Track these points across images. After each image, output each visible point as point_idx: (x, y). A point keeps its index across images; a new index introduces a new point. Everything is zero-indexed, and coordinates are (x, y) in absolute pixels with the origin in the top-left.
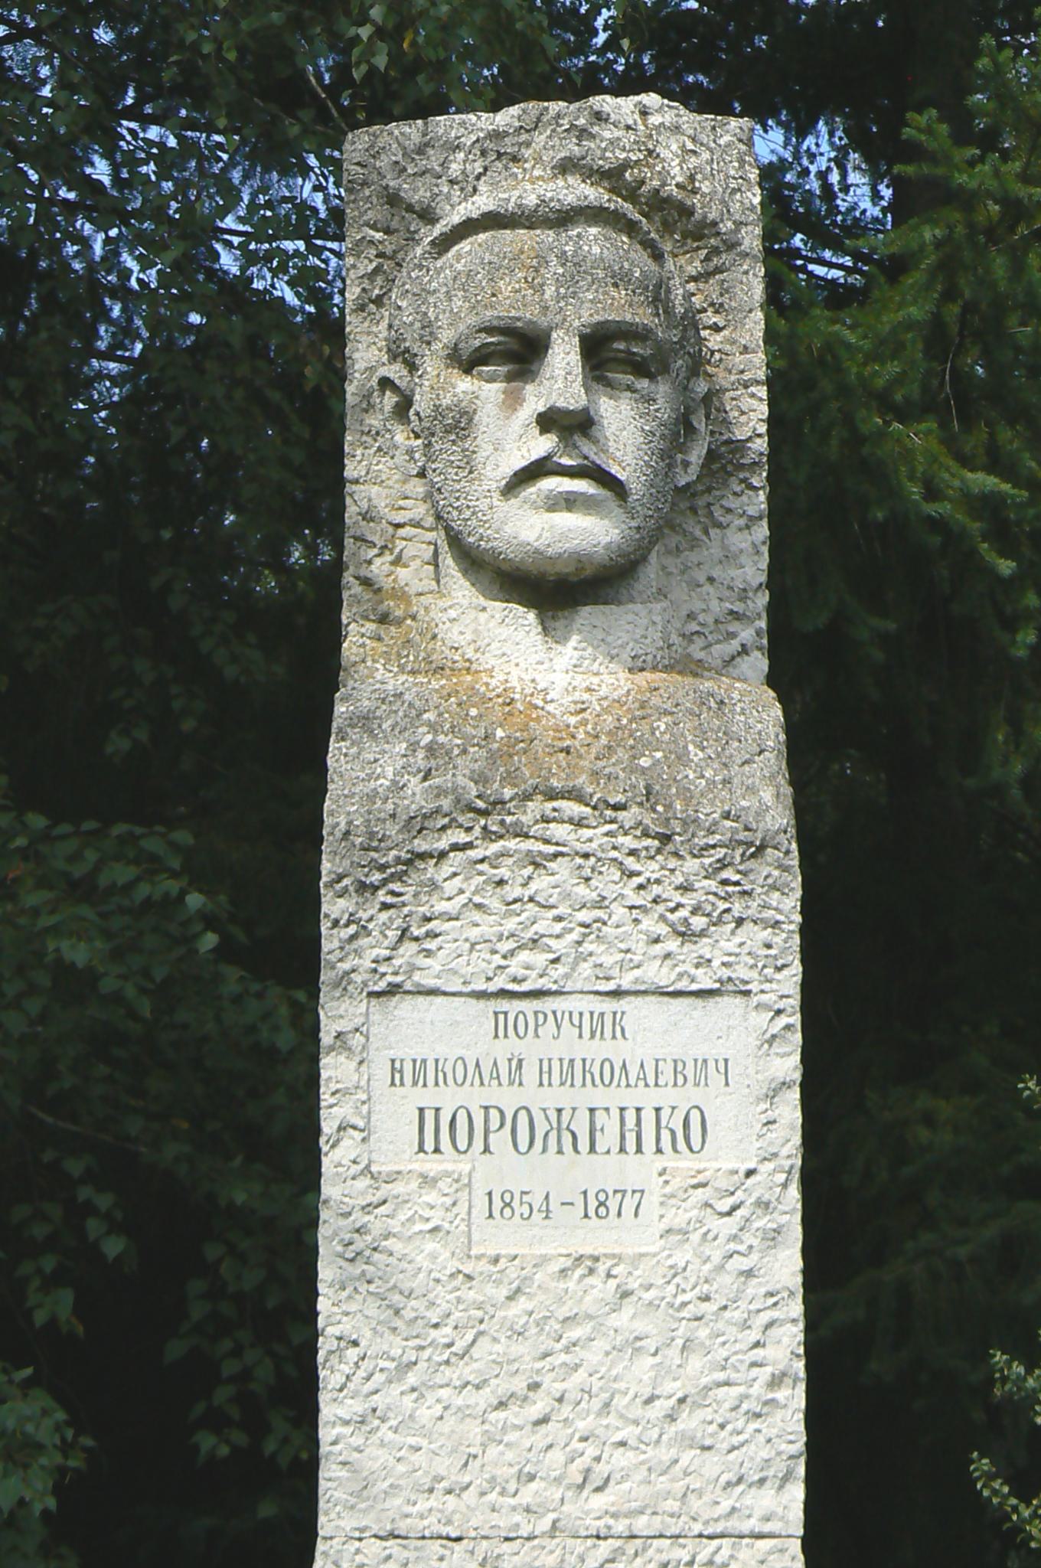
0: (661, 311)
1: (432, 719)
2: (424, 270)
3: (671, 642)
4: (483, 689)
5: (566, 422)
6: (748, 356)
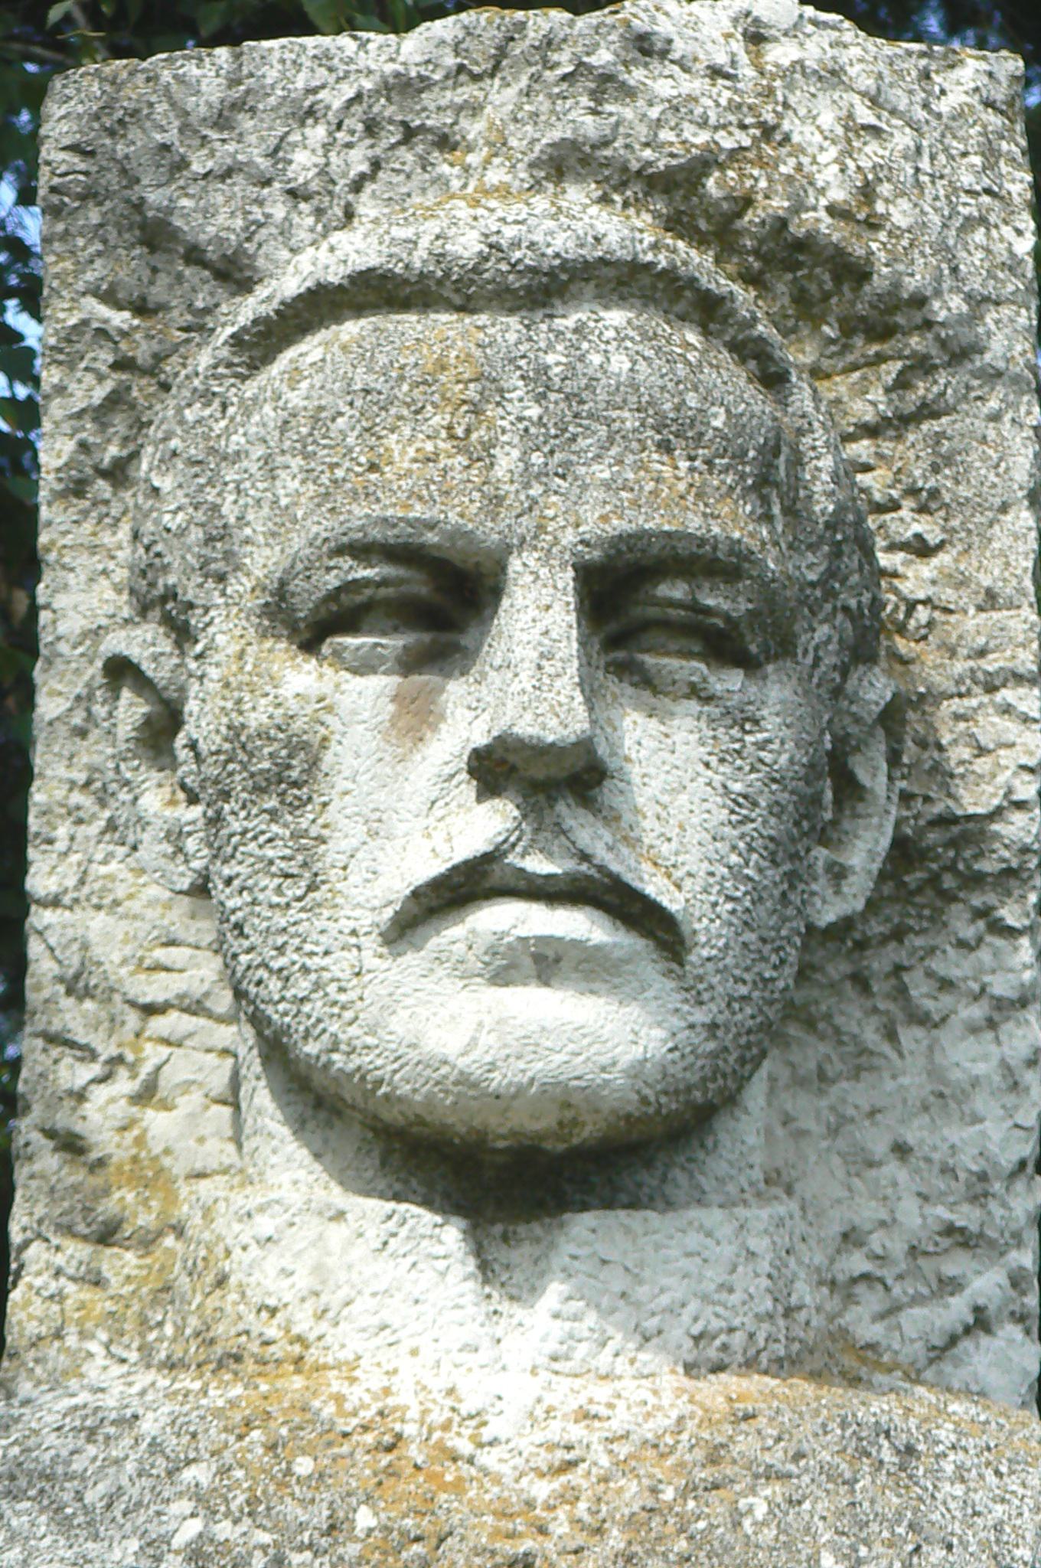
0: (776, 510)
1: (205, 1481)
2: (216, 404)
3: (794, 1300)
4: (329, 1410)
5: (539, 773)
6: (996, 615)
